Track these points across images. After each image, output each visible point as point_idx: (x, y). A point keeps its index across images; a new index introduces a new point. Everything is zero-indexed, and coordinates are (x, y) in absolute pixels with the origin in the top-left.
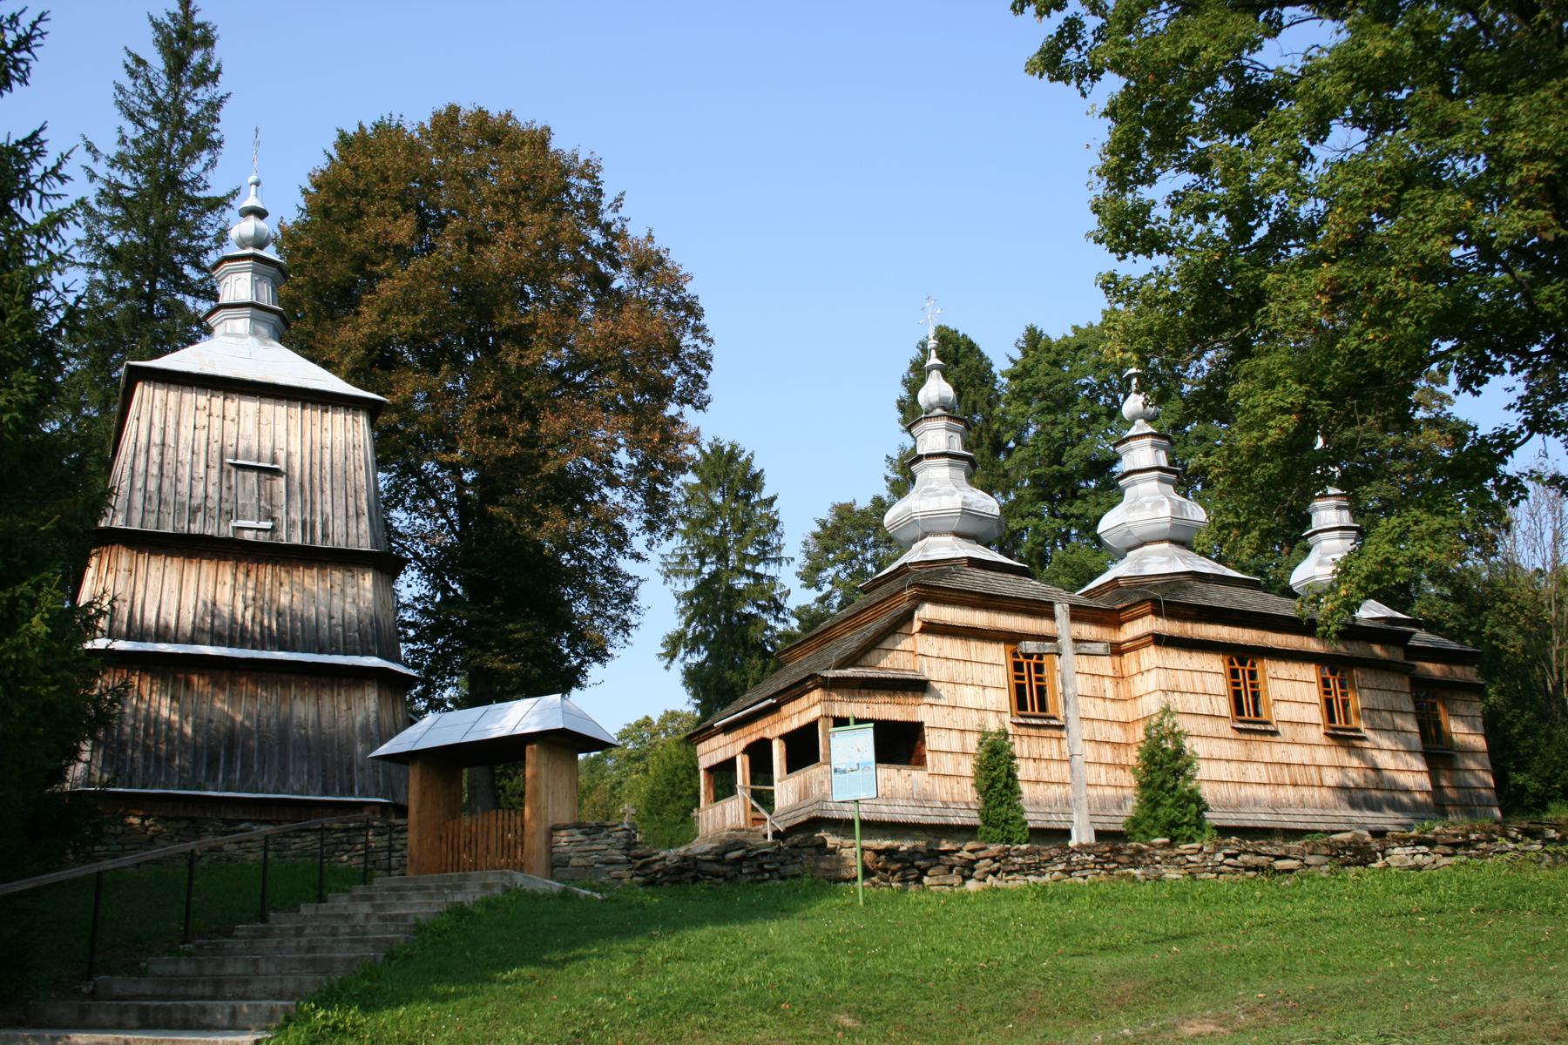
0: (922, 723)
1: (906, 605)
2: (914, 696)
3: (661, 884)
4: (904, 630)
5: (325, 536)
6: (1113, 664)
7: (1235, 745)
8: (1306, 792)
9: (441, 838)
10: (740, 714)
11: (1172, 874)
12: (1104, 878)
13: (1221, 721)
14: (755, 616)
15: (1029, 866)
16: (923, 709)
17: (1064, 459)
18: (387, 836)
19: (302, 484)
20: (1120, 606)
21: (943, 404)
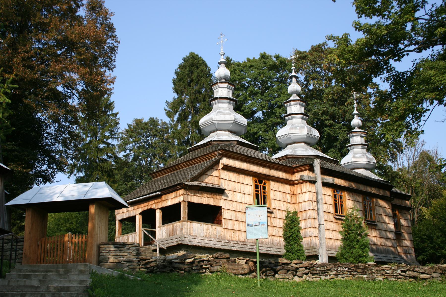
0: (221, 207)
1: (217, 158)
2: (219, 195)
3: (156, 273)
4: (215, 168)
6: (291, 189)
7: (335, 224)
9: (38, 246)
10: (141, 198)
11: (379, 278)
12: (351, 278)
13: (330, 215)
14: (106, 160)
15: (322, 271)
16: (222, 201)
17: (242, 109)
18: (10, 244)
20: (295, 166)
21: (226, 78)
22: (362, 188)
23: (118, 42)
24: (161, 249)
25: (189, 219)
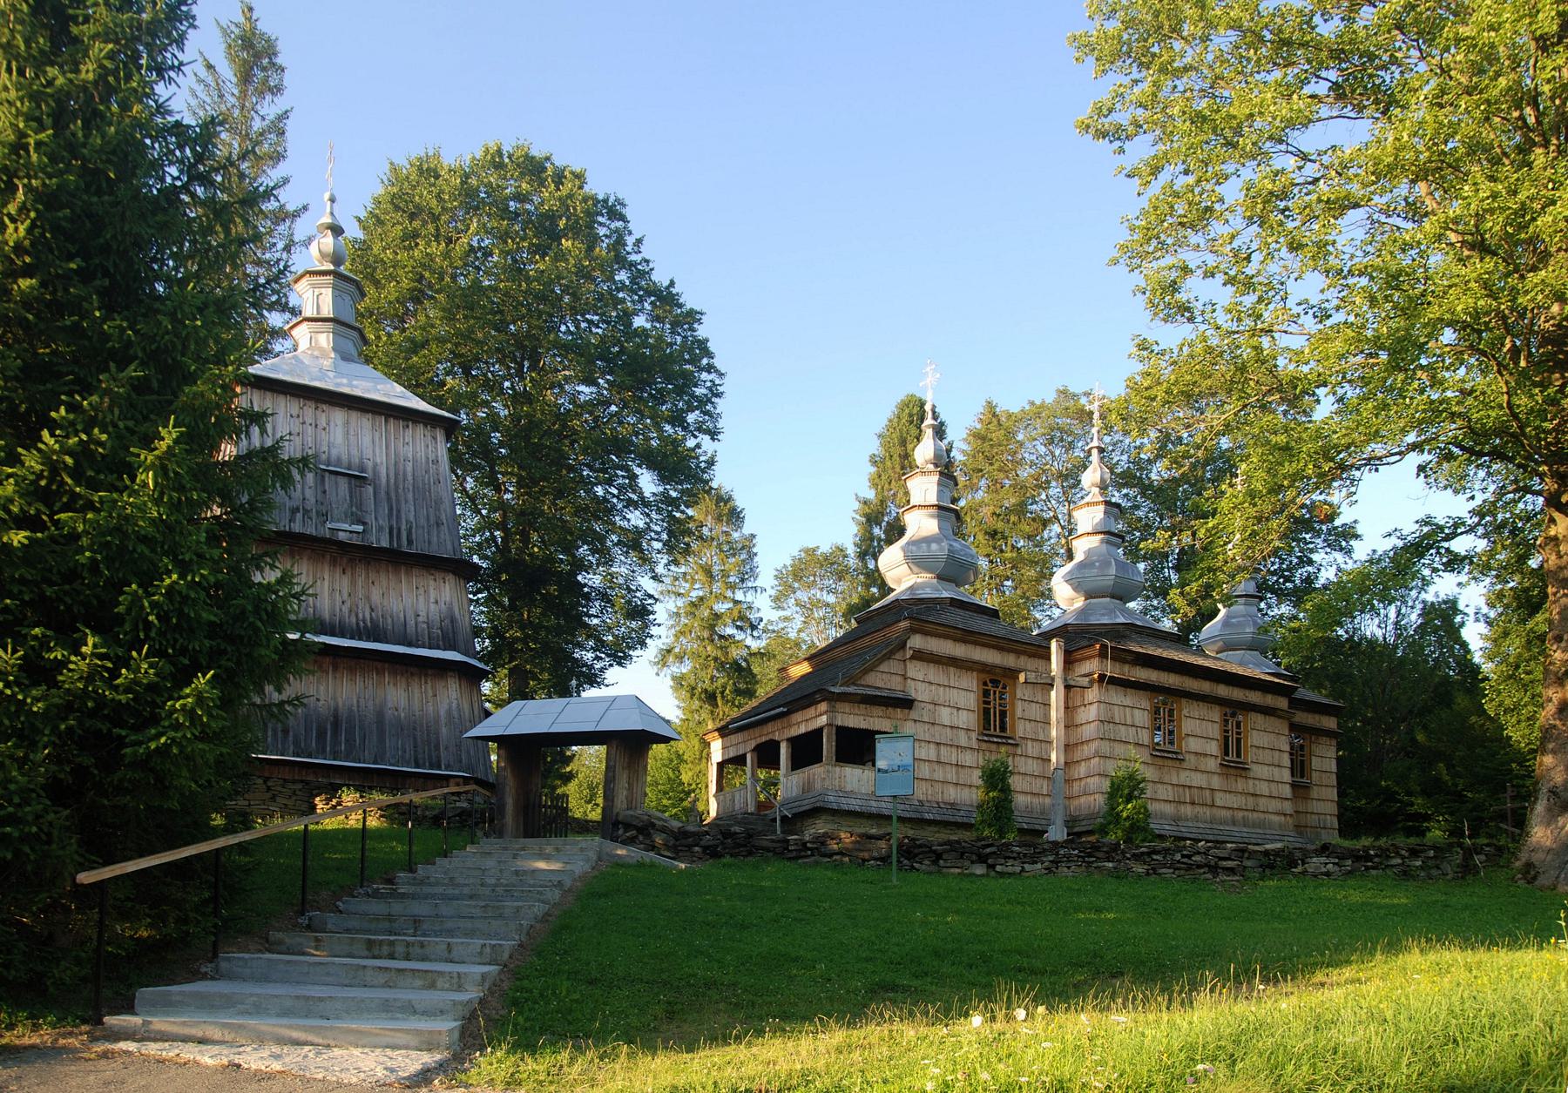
5: (410, 542)
8: (1198, 809)
19: (388, 493)
22: (1223, 691)
23: (721, 375)
24: (784, 819)
25: (838, 760)
